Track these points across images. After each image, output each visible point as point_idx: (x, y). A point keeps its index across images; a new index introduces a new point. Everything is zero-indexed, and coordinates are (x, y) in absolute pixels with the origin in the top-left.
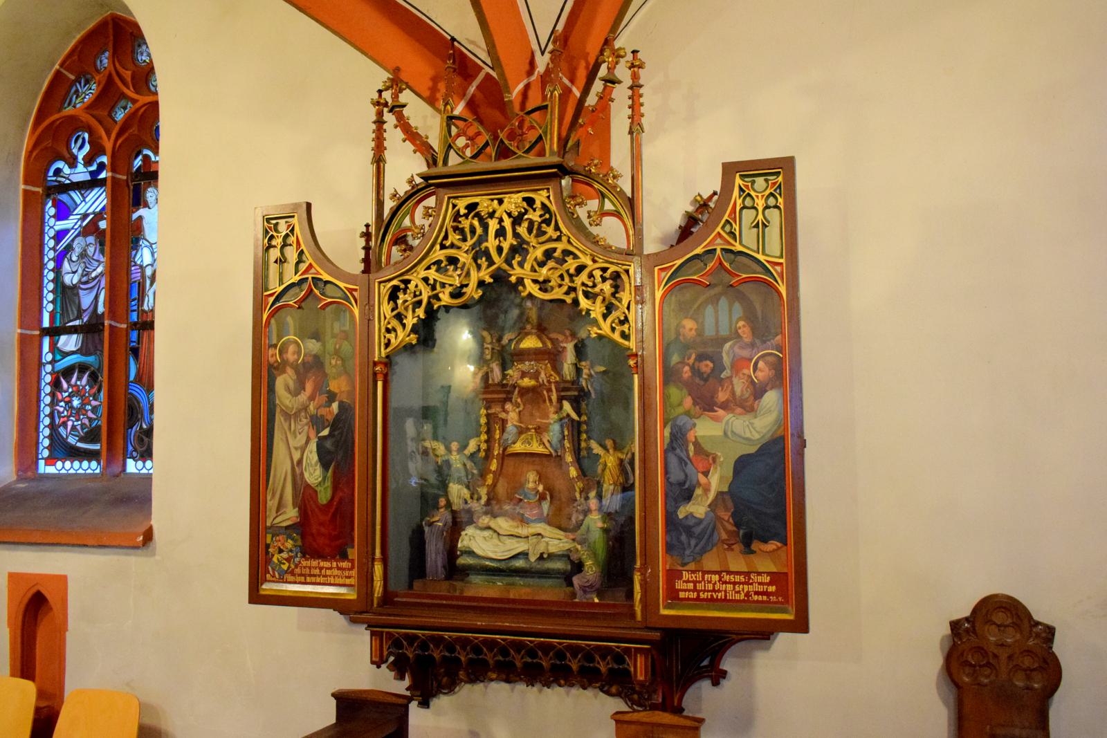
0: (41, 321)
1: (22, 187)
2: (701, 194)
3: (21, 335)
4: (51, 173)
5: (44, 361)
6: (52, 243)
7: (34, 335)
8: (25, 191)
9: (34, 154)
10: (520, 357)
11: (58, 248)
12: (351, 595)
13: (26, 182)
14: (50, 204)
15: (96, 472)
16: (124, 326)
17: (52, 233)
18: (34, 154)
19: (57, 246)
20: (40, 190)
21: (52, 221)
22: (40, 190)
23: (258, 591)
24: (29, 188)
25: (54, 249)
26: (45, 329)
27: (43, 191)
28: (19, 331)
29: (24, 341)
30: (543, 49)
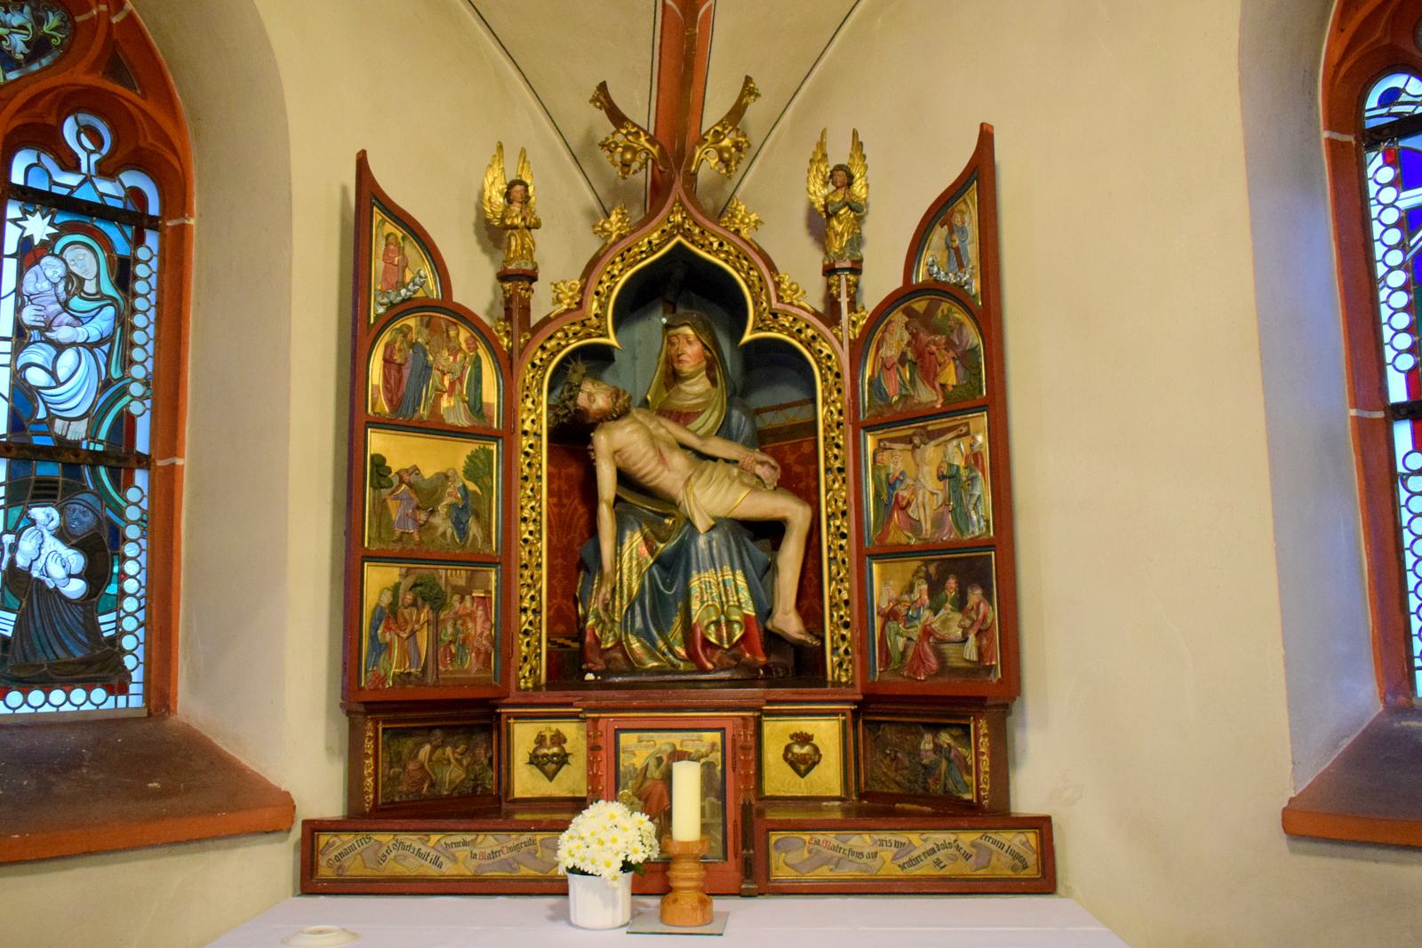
0: (1383, 390)
1: (1325, 134)
2: (828, 132)
3: (1357, 419)
4: (1372, 101)
5: (1400, 469)
6: (1394, 236)
7: (1374, 421)
8: (1331, 142)
9: (1343, 70)
10: (1407, 677)
11: (1412, 242)
12: (380, 803)
13: (1332, 125)
14: (1379, 161)
15: (144, 547)
16: (1380, 415)
17: (1391, 216)
18: (1343, 70)
19: (1411, 238)
20: (1350, 138)
21: (1388, 195)
22: (1350, 138)
23: (768, 880)
24: (1336, 136)
25: (1402, 246)
26: (1398, 406)
27: (1356, 139)
28: (1353, 412)
29: (1363, 427)
30: (19, 222)
